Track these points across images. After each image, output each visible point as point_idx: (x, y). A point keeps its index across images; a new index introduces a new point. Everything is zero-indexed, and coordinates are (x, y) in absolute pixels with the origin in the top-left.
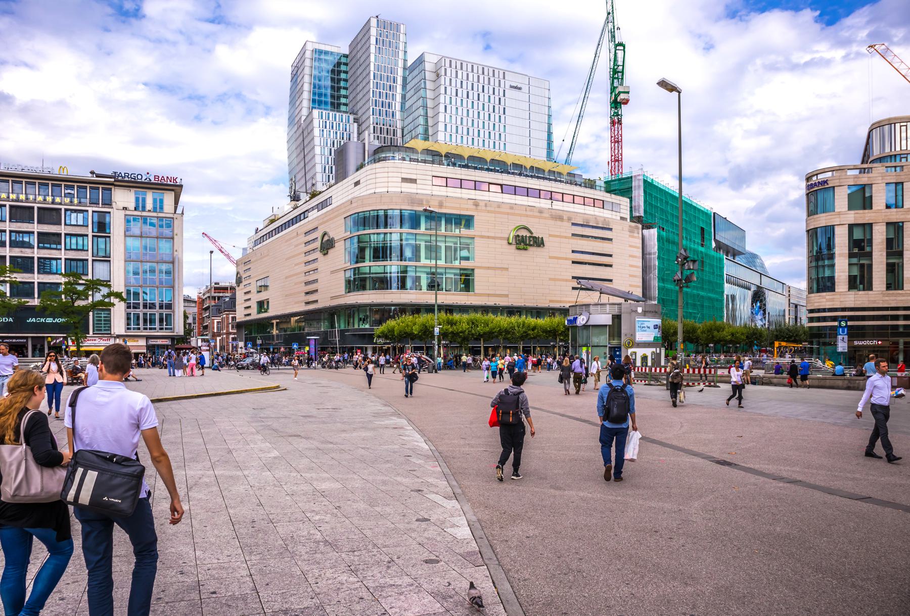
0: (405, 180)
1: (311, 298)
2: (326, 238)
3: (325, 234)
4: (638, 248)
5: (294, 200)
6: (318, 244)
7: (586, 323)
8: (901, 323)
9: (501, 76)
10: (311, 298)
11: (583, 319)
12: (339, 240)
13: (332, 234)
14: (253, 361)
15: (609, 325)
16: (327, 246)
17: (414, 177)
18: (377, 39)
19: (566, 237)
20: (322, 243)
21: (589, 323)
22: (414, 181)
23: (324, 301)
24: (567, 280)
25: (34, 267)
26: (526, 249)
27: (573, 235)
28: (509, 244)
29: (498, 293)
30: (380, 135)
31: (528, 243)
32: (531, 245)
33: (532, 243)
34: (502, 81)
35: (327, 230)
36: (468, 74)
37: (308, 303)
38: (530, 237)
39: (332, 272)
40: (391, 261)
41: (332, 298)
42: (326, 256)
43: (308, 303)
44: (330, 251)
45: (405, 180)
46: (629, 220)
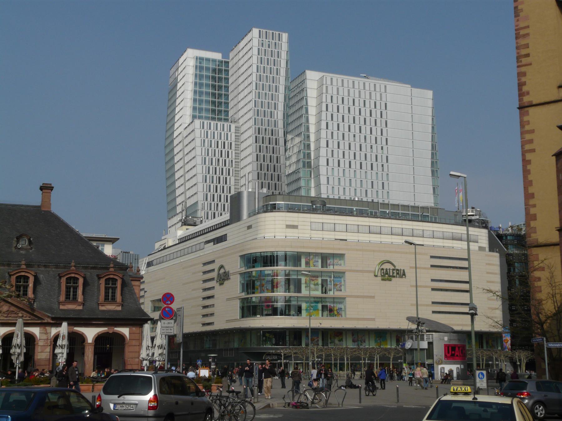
0: (288, 226)
1: (208, 320)
2: (222, 271)
3: (222, 267)
4: (496, 274)
5: (185, 225)
6: (214, 275)
7: (411, 347)
8: (375, 362)
9: (383, 90)
10: (208, 320)
11: (409, 344)
12: (234, 274)
13: (227, 268)
14: (81, 378)
15: (426, 349)
16: (223, 278)
17: (295, 224)
18: (258, 66)
19: (425, 268)
20: (219, 274)
21: (413, 348)
22: (295, 227)
23: (220, 324)
24: (427, 305)
25: (434, 403)
26: (390, 280)
27: (432, 266)
28: (376, 276)
29: (365, 317)
30: (267, 173)
31: (391, 274)
32: (394, 277)
33: (395, 275)
34: (384, 95)
35: (224, 264)
36: (349, 90)
37: (204, 324)
38: (393, 270)
39: (228, 299)
40: (277, 266)
41: (228, 321)
42: (222, 286)
43: (204, 324)
44: (226, 282)
45: (288, 226)
46: (487, 249)
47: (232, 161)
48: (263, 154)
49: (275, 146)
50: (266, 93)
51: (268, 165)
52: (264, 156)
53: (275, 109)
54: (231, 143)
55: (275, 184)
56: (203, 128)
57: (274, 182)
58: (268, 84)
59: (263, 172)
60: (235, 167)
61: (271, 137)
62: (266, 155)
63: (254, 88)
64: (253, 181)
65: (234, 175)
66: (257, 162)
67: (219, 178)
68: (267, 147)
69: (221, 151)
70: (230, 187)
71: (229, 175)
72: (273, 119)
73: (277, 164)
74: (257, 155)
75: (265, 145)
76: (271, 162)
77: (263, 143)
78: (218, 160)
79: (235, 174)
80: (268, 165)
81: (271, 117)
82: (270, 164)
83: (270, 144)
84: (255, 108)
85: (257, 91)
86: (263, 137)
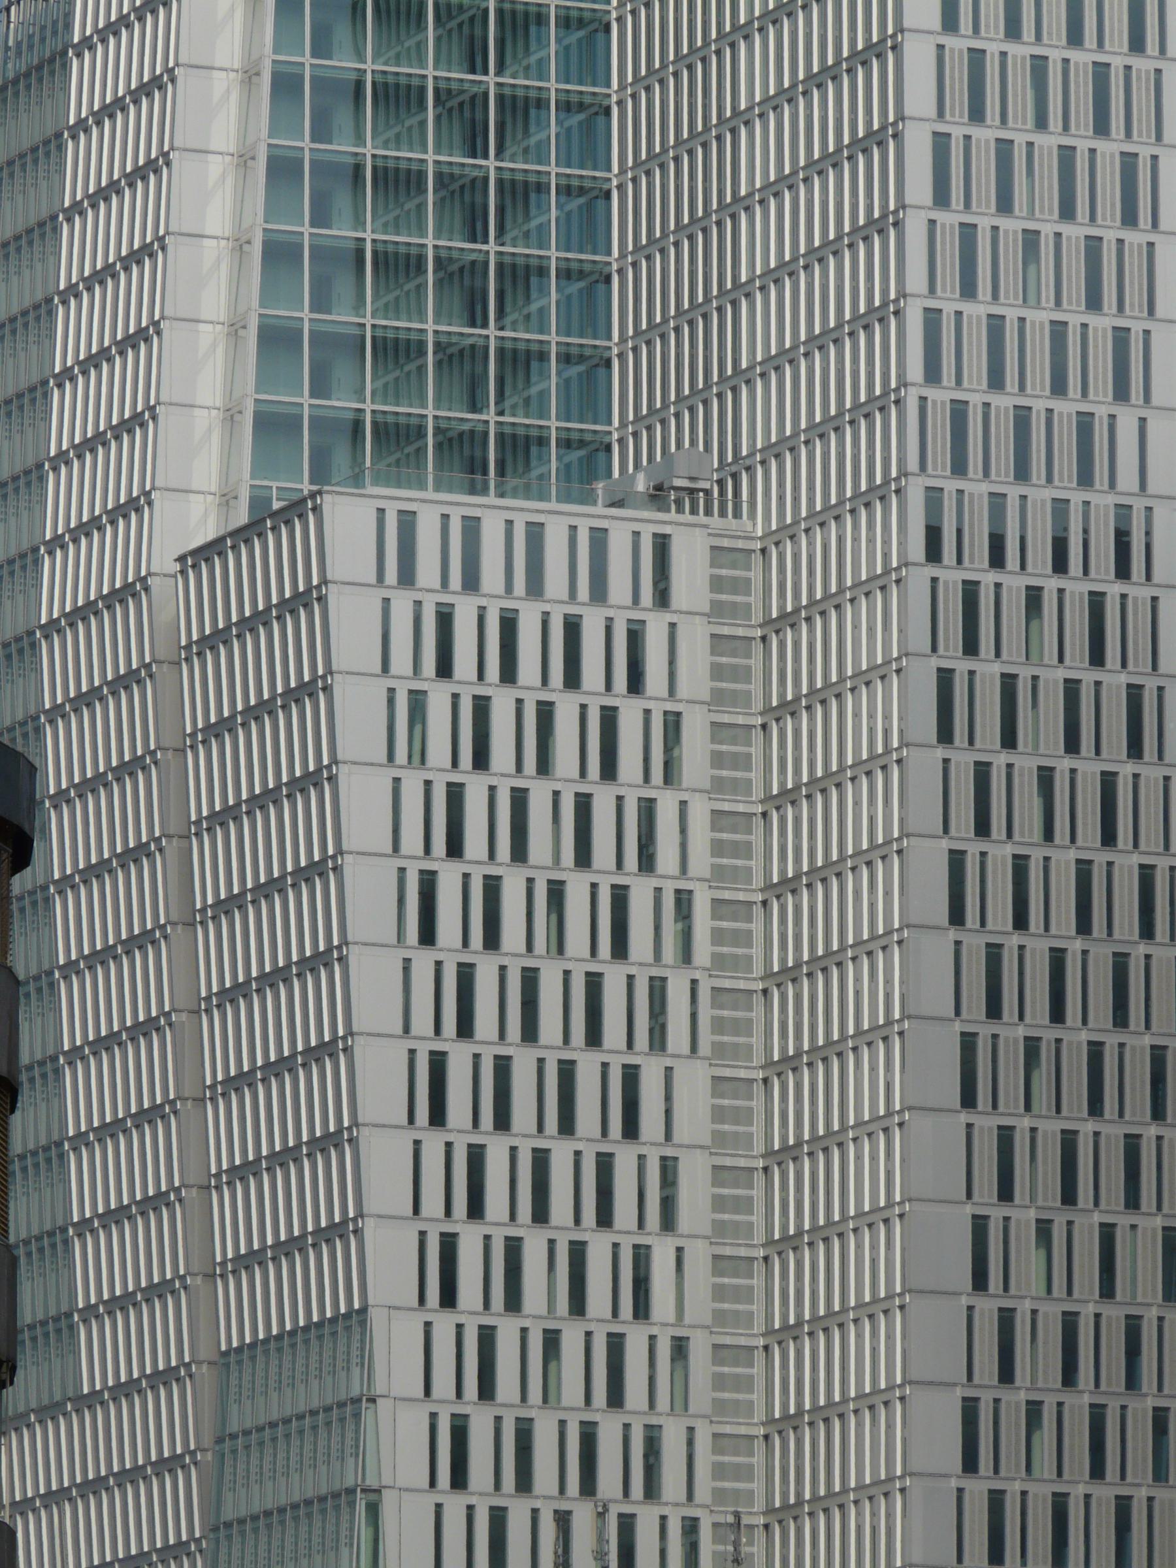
30: (1049, 1034)
47: (684, 901)
48: (1009, 850)
49: (1126, 770)
50: (1031, 239)
51: (1058, 958)
52: (1020, 865)
53: (1121, 393)
54: (673, 723)
55: (1132, 1145)
56: (407, 577)
57: (1113, 1132)
58: (1048, 142)
59: (1013, 1033)
60: (719, 961)
61: (1088, 677)
62: (1037, 856)
63: (920, 187)
64: (921, 1124)
65: (704, 1048)
66: (952, 934)
67: (567, 1071)
68: (1046, 777)
69: (584, 805)
70: (668, 1168)
71: (658, 1038)
72: (1103, 501)
73: (1142, 949)
74: (956, 860)
75: (1026, 763)
76: (1084, 926)
77: (1009, 740)
78: (556, 892)
79: (719, 1025)
80: (1058, 958)
81: (1085, 478)
82: (1076, 946)
83: (1072, 745)
84: (932, 393)
85: (949, 219)
86: (1009, 683)
